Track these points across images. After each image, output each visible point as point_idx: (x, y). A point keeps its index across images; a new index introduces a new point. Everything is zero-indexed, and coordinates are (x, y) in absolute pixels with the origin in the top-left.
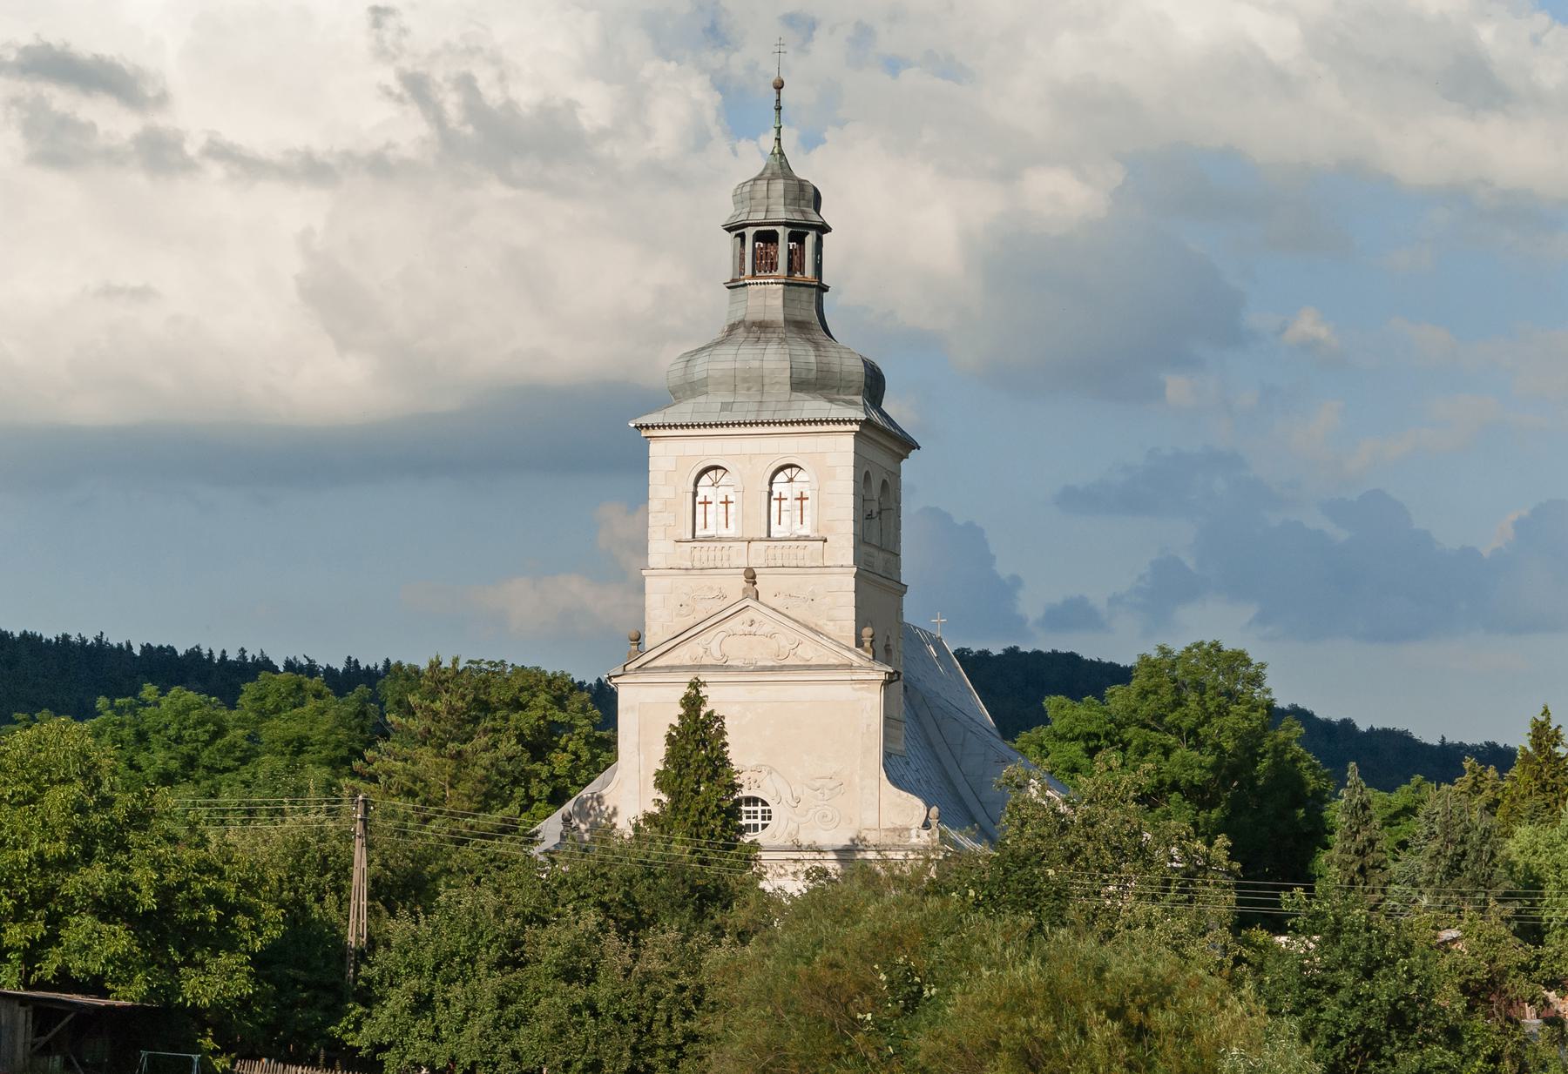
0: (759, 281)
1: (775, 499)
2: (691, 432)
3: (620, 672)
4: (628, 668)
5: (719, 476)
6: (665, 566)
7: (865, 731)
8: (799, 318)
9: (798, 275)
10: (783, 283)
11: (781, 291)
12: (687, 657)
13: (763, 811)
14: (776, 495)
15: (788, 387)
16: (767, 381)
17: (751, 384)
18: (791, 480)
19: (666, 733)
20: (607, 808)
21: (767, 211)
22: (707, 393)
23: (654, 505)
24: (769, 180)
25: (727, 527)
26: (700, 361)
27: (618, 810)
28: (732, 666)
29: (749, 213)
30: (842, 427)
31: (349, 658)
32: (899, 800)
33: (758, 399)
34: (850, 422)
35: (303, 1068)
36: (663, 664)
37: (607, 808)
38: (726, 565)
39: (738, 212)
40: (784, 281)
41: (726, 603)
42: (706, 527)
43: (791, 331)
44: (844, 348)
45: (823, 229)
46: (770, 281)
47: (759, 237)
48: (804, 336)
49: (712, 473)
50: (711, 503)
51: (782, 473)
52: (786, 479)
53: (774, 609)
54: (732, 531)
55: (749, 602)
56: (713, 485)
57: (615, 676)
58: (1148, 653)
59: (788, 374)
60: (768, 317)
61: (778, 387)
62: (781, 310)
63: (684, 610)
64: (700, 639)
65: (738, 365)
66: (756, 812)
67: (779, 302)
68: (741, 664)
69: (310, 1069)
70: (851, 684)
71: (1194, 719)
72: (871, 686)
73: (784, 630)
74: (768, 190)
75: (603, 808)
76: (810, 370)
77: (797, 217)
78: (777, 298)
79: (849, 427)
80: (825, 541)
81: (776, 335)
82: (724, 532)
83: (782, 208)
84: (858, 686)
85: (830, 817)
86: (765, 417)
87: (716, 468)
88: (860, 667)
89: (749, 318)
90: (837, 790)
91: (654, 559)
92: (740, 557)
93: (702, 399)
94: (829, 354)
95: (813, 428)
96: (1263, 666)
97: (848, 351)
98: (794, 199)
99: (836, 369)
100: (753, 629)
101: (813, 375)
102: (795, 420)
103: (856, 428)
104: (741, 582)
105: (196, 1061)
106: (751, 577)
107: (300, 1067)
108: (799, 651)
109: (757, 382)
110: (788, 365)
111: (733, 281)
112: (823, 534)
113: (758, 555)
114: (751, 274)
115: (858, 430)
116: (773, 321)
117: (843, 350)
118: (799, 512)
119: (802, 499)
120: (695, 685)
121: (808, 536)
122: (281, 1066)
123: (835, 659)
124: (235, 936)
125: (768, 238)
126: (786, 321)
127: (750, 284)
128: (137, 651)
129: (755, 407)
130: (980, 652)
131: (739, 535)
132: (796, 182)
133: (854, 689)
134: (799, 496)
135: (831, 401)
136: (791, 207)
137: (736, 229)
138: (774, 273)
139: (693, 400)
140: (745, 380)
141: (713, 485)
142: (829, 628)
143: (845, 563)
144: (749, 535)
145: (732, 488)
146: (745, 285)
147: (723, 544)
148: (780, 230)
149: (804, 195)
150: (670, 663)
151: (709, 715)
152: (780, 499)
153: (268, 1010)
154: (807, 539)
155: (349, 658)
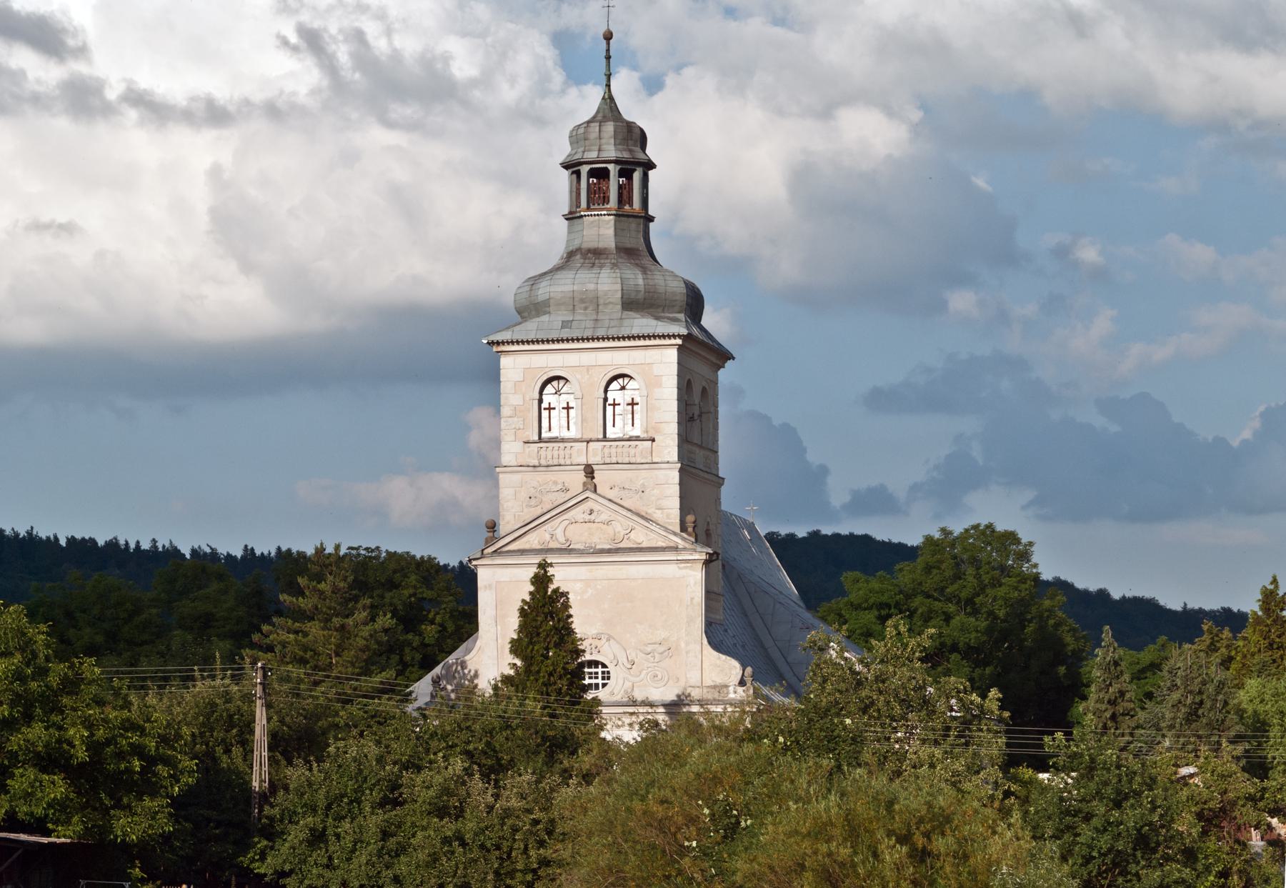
0: (593, 213)
1: (609, 405)
3: (478, 555)
4: (486, 551)
5: (561, 385)
6: (516, 464)
7: (689, 603)
8: (628, 246)
9: (627, 207)
11: (613, 222)
12: (536, 542)
13: (603, 673)
14: (610, 401)
15: (619, 307)
16: (601, 301)
18: (623, 388)
19: (518, 607)
22: (549, 313)
23: (505, 411)
29: (584, 152)
31: (246, 546)
32: (718, 662)
34: (674, 336)
38: (568, 462)
39: (574, 152)
40: (614, 212)
41: (569, 495)
42: (550, 430)
43: (621, 258)
45: (650, 165)
46: (603, 213)
47: (592, 173)
49: (555, 383)
50: (554, 409)
51: (549, 385)
52: (619, 387)
53: (610, 500)
54: (573, 433)
55: (588, 494)
56: (556, 393)
57: (475, 559)
59: (619, 295)
60: (601, 245)
61: (611, 306)
62: (613, 239)
63: (533, 502)
64: (547, 527)
65: (576, 288)
66: (597, 673)
67: (611, 232)
68: (582, 547)
72: (694, 565)
75: (466, 671)
76: (638, 292)
77: (626, 155)
78: (609, 228)
79: (673, 341)
82: (565, 434)
83: (612, 147)
84: (683, 565)
85: (660, 677)
86: (600, 333)
88: (685, 549)
89: (585, 246)
90: (666, 653)
91: (507, 459)
92: (580, 455)
93: (545, 318)
95: (642, 342)
98: (624, 139)
99: (661, 290)
100: (592, 517)
101: (641, 296)
103: (679, 341)
104: (581, 477)
106: (589, 471)
108: (632, 535)
109: (593, 302)
111: (571, 213)
112: (651, 434)
113: (595, 454)
116: (606, 249)
118: (630, 416)
120: (543, 566)
121: (639, 437)
126: (617, 248)
127: (585, 216)
128: (63, 542)
129: (590, 324)
130: (787, 535)
131: (579, 436)
132: (625, 124)
133: (680, 568)
135: (657, 318)
137: (571, 166)
138: (606, 206)
139: (538, 319)
140: (582, 301)
141: (556, 393)
142: (658, 515)
143: (670, 460)
145: (572, 396)
147: (566, 444)
148: (611, 167)
150: (521, 547)
154: (637, 439)
155: (246, 546)
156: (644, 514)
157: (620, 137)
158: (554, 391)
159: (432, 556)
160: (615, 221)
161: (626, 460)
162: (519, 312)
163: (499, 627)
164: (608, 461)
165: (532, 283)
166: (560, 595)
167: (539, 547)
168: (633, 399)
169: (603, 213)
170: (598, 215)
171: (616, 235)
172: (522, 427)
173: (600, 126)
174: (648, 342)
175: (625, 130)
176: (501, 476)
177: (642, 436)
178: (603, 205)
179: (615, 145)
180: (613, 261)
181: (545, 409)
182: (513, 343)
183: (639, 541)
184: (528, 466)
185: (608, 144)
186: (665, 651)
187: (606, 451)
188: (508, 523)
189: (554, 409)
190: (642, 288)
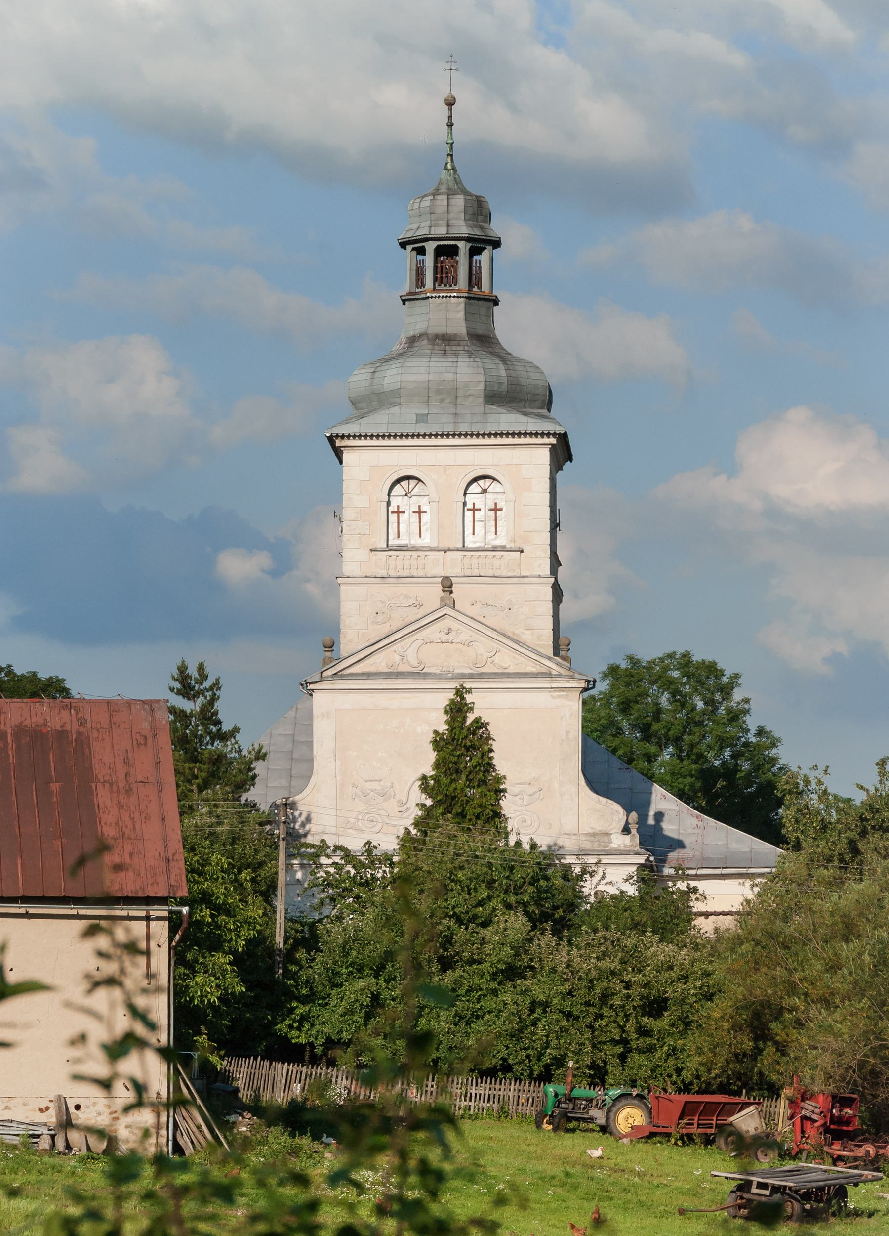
0: (441, 295)
1: (468, 510)
2: (386, 442)
3: (317, 678)
4: (325, 674)
5: (411, 486)
6: (359, 574)
7: (564, 738)
8: (480, 332)
9: (475, 289)
10: (465, 297)
11: (463, 305)
12: (383, 664)
14: (469, 505)
15: (481, 400)
16: (460, 393)
17: (444, 396)
18: (485, 491)
20: (300, 815)
21: (448, 226)
22: (400, 404)
23: (348, 514)
24: (448, 195)
25: (420, 537)
26: (389, 372)
27: (312, 816)
28: (430, 673)
29: (430, 227)
30: (539, 440)
33: (453, 410)
34: (548, 435)
35: (289, 1065)
36: (360, 671)
37: (300, 815)
38: (422, 574)
40: (466, 295)
41: (421, 612)
42: (399, 537)
44: (528, 362)
46: (453, 295)
47: (440, 252)
48: (487, 350)
49: (404, 484)
50: (404, 512)
51: (398, 485)
52: (480, 490)
53: (472, 618)
54: (427, 540)
55: (447, 610)
56: (406, 495)
57: (311, 683)
58: (618, 663)
59: (481, 386)
60: (450, 330)
61: (471, 399)
62: (463, 324)
63: (380, 618)
64: (396, 647)
65: (431, 377)
67: (461, 315)
68: (438, 672)
69: (296, 1066)
70: (550, 692)
71: (680, 729)
73: (482, 639)
74: (448, 205)
75: (297, 813)
76: (501, 383)
77: (477, 232)
78: (459, 311)
79: (546, 440)
80: (522, 551)
81: (461, 348)
82: (416, 541)
83: (462, 223)
85: (529, 822)
86: (463, 429)
87: (408, 478)
88: (560, 675)
89: (432, 331)
90: (537, 795)
91: (349, 568)
92: (437, 566)
93: (396, 410)
94: (516, 367)
95: (510, 441)
96: (737, 676)
97: (531, 365)
98: (474, 214)
99: (524, 382)
100: (450, 637)
101: (504, 388)
102: (534, 432)
103: (553, 441)
104: (437, 590)
105: (196, 1057)
106: (447, 585)
107: (286, 1064)
108: (497, 659)
110: (482, 378)
112: (519, 544)
113: (453, 564)
114: (432, 287)
115: (555, 442)
116: (456, 334)
117: (528, 365)
119: (496, 509)
120: (460, 692)
121: (504, 547)
122: (267, 1063)
123: (532, 667)
124: (220, 935)
125: (447, 252)
126: (469, 334)
127: (432, 297)
131: (434, 544)
132: (474, 198)
133: (553, 697)
134: (494, 507)
135: (525, 414)
136: (471, 223)
138: (454, 287)
139: (387, 411)
140: (438, 392)
141: (406, 495)
142: (527, 637)
143: (542, 574)
144: (446, 545)
145: (426, 499)
146: (428, 298)
147: (419, 553)
148: (461, 244)
149: (481, 211)
150: (366, 670)
151: (477, 720)
152: (474, 510)
153: (232, 1009)
154: (503, 549)
156: (511, 635)
157: (470, 212)
158: (404, 493)
159: (60, 677)
160: (466, 304)
161: (491, 573)
162: (354, 403)
163: (338, 762)
164: (468, 573)
165: (373, 370)
166: (479, 724)
167: (386, 670)
168: (496, 504)
169: (453, 295)
170: (446, 297)
171: (466, 320)
172: (367, 532)
173: (448, 199)
174: (517, 440)
175: (476, 205)
176: (343, 587)
177: (508, 546)
178: (451, 286)
179: (465, 220)
180: (466, 348)
181: (393, 512)
182: (360, 437)
183: (506, 666)
184: (376, 577)
185: (457, 219)
186: (535, 793)
187: (466, 561)
188: (350, 642)
189: (404, 512)
190: (505, 380)
